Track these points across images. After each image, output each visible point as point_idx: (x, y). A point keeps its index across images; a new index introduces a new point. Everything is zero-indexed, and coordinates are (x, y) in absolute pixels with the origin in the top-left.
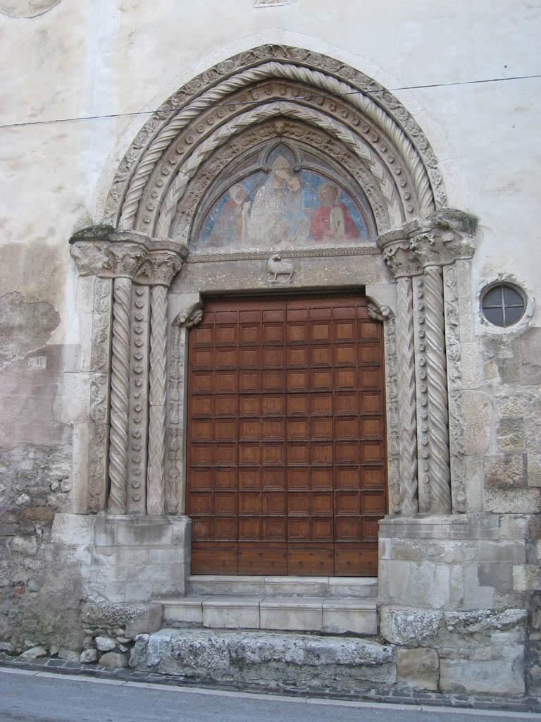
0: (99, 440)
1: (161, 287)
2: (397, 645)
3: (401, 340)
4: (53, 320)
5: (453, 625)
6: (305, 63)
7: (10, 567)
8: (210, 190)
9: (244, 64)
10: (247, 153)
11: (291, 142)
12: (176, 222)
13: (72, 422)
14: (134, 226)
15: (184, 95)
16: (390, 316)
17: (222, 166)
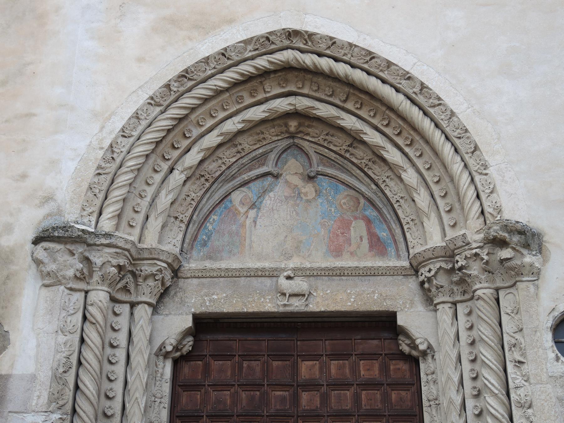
1: (146, 306)
3: (446, 382)
6: (328, 52)
8: (208, 195)
9: (257, 49)
10: (254, 154)
11: (305, 144)
12: (167, 229)
15: (186, 80)
16: (428, 351)
17: (224, 167)
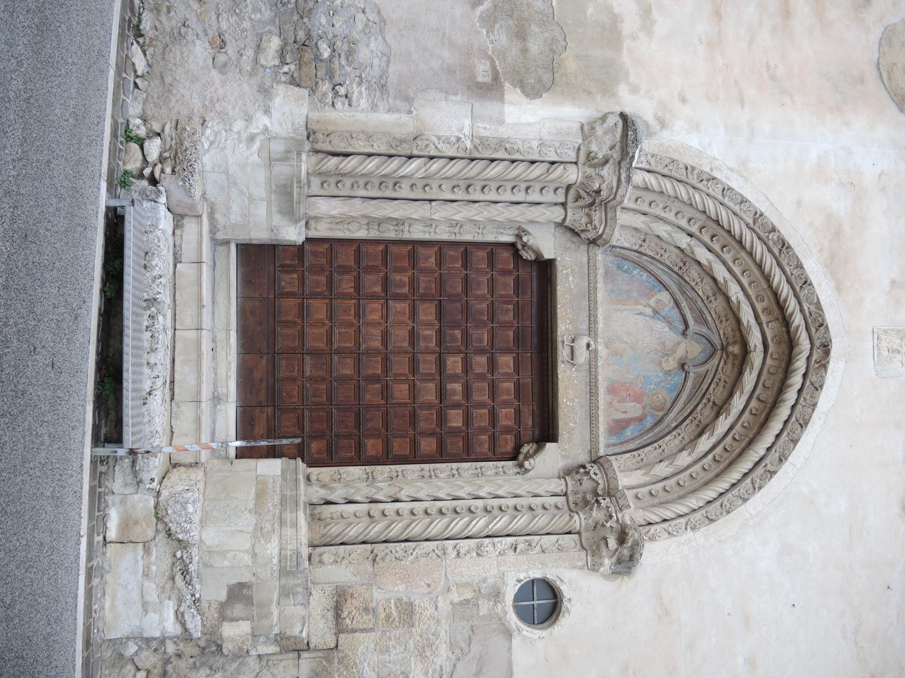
0: (394, 144)
1: (563, 217)
2: (159, 493)
3: (498, 484)
4: (533, 91)
5: (182, 557)
6: (808, 383)
7: (243, 31)
8: (666, 269)
9: (811, 315)
10: (706, 312)
11: (715, 361)
12: (634, 233)
13: (415, 112)
14: (636, 187)
15: (780, 247)
16: (523, 469)
17: (693, 284)
